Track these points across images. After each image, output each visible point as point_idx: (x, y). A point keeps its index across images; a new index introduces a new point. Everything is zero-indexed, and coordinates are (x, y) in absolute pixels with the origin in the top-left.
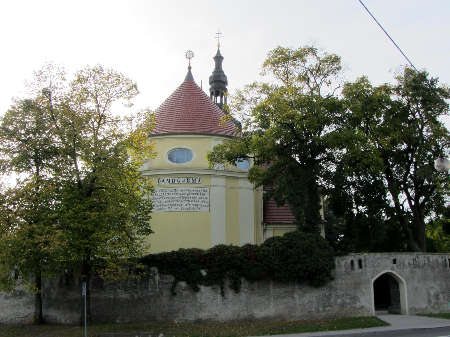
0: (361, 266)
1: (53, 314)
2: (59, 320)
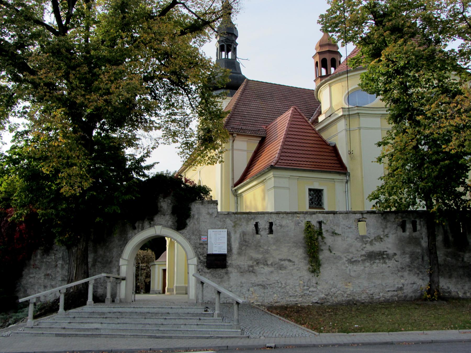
0: (271, 232)
1: (446, 284)
2: (453, 294)
